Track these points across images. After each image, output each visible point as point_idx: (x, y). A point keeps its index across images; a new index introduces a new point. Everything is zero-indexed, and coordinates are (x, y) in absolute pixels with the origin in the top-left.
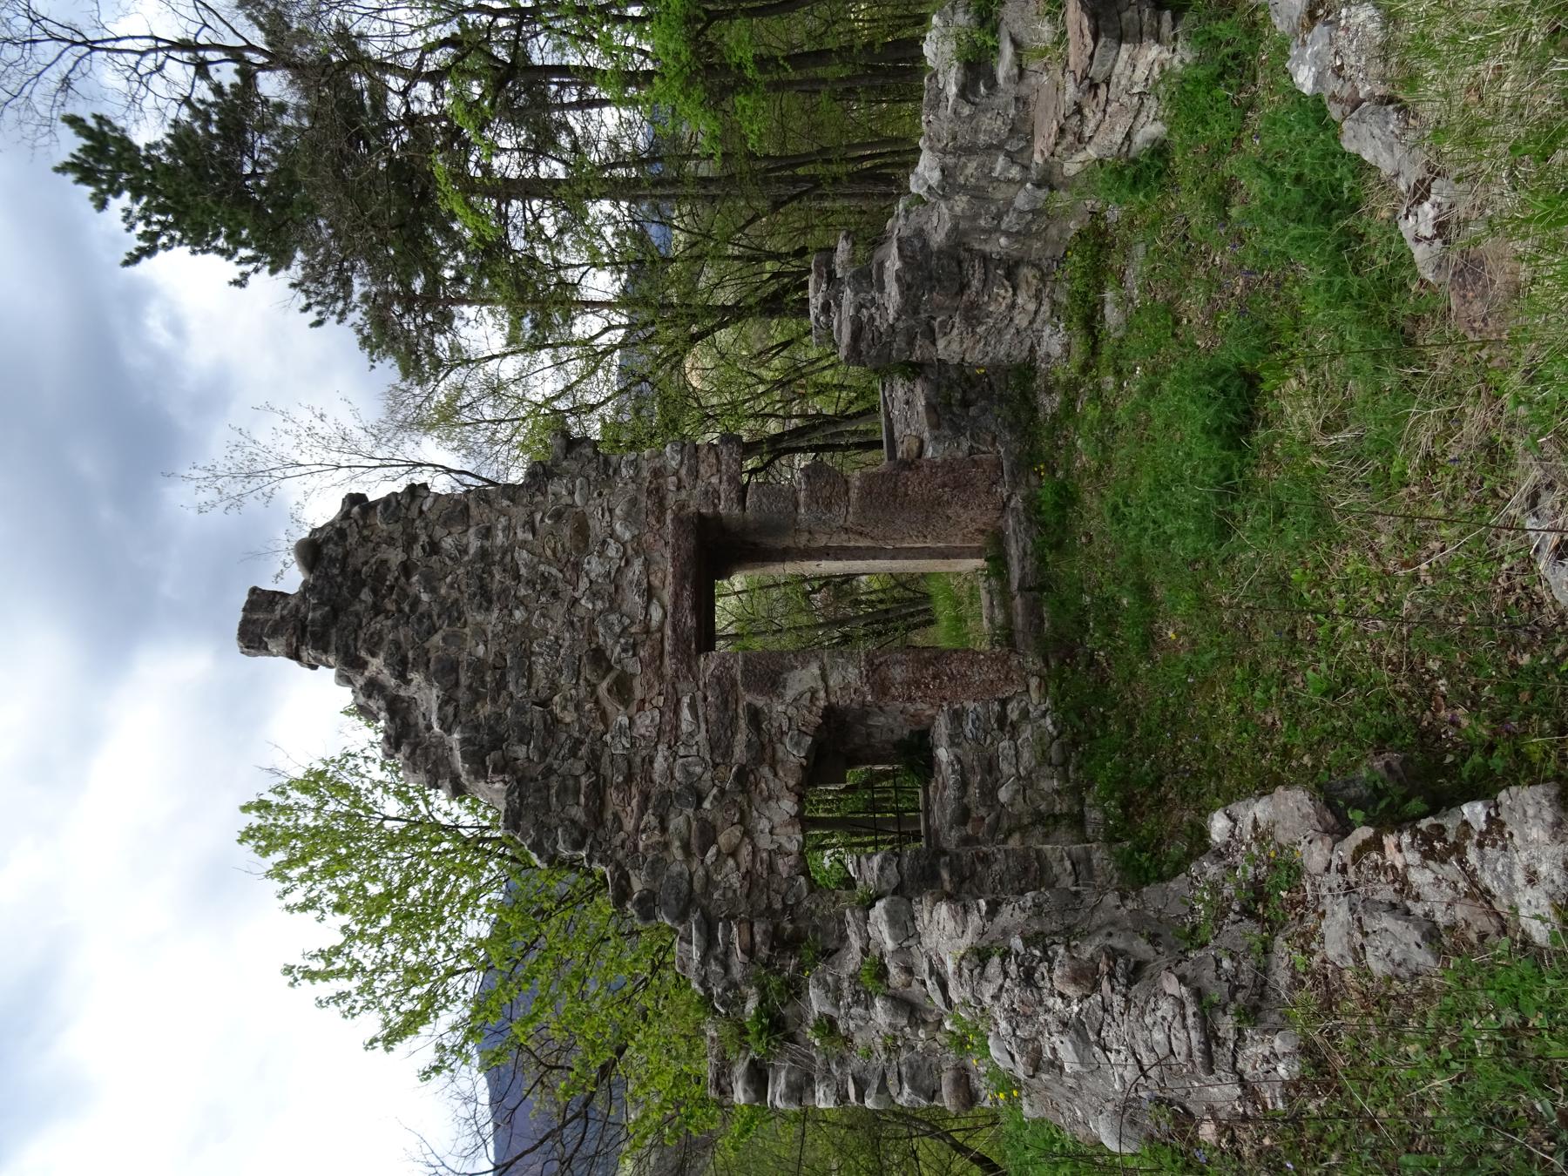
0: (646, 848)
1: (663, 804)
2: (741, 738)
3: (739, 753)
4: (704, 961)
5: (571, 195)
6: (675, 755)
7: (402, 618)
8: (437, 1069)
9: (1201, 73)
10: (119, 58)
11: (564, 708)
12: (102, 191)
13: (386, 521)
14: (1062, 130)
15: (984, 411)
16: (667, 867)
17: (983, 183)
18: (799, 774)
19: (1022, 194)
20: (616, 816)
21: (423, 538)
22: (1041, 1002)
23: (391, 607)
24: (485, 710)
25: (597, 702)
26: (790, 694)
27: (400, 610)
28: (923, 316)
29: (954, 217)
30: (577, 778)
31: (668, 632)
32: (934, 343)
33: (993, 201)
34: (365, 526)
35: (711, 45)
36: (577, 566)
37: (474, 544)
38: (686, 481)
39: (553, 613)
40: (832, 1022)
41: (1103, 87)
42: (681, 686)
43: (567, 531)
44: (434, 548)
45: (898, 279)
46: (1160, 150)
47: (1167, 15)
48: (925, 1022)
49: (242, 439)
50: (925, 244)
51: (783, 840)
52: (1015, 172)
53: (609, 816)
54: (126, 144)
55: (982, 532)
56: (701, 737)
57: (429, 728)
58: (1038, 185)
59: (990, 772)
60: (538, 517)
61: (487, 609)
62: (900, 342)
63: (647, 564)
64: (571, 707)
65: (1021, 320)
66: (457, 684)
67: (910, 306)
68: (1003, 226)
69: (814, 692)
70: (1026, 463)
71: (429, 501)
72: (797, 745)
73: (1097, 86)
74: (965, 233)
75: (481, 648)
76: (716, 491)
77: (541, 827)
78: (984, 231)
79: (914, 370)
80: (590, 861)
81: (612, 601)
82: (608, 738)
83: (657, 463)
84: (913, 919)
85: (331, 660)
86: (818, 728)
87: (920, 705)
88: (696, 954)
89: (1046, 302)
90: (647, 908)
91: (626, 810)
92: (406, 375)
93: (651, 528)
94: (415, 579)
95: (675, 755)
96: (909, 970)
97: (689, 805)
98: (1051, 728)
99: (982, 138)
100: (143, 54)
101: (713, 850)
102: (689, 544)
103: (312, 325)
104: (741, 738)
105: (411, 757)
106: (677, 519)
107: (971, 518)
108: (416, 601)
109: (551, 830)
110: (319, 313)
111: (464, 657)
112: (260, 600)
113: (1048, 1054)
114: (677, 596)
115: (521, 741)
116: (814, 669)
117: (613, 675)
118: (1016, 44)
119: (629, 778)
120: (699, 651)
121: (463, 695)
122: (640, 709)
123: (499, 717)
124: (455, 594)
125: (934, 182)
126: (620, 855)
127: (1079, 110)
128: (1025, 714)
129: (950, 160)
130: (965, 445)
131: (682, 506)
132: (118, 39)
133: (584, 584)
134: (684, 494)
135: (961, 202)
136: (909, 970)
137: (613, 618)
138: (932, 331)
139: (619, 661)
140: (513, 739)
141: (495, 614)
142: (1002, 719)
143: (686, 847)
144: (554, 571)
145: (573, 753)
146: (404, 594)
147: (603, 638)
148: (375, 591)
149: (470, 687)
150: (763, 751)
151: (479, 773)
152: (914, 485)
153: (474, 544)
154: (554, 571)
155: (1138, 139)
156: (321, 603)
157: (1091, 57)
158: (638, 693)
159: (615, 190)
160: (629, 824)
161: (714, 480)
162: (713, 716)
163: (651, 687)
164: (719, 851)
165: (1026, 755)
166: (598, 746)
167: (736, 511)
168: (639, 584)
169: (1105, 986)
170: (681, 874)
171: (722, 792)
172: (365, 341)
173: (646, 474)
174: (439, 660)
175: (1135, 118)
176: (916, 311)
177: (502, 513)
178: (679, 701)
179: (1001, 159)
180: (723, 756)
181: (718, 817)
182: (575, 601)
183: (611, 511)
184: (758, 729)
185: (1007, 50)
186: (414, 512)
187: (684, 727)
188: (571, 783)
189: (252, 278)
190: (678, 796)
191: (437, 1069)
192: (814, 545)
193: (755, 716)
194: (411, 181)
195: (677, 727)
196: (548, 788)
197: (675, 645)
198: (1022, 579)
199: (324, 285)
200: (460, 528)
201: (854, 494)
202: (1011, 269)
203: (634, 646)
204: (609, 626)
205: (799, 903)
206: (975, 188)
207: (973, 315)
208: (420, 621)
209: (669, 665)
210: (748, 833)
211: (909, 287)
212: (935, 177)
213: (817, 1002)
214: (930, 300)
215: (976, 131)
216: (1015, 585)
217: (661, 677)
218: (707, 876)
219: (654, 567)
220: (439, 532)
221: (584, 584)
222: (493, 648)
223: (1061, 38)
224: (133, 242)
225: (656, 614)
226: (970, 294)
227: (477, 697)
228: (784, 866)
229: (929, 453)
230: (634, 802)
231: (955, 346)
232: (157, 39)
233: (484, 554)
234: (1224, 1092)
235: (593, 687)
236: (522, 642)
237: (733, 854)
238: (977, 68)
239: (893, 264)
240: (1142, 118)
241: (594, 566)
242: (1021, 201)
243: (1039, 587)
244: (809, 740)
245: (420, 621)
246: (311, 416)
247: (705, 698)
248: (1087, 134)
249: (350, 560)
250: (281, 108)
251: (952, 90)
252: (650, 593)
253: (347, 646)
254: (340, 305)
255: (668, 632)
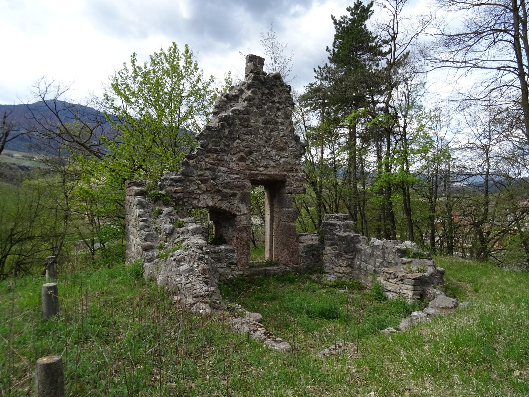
0: (201, 164)
1: (212, 169)
2: (229, 191)
3: (225, 191)
4: (171, 179)
5: (350, 146)
6: (224, 173)
7: (261, 100)
8: (107, 98)
9: (406, 305)
10: (392, 22)
11: (237, 143)
12: (352, 10)
13: (285, 97)
14: (390, 274)
15: (311, 260)
16: (196, 170)
17: (375, 256)
18: (219, 207)
19: (372, 266)
20: (209, 156)
21: (281, 107)
22: (195, 262)
23: (264, 98)
24: (237, 122)
25: (239, 152)
26: (240, 205)
27: (263, 100)
28: (338, 242)
29: (365, 250)
30: (219, 146)
31: (256, 172)
32: (330, 246)
33: (369, 259)
34: (284, 92)
35: (397, 189)
36: (273, 148)
37: (280, 120)
38: (294, 178)
39: (262, 141)
40: (161, 214)
41: (401, 282)
42: (242, 175)
43: (282, 145)
44: (279, 109)
45: (349, 235)
46: (386, 298)
47: (419, 297)
48: (167, 238)
49: (283, 47)
50: (357, 243)
51: (202, 202)
52: (378, 264)
53: (209, 154)
54: (367, 18)
55: (278, 260)
56: (229, 180)
57: (231, 106)
58: (374, 271)
59: (218, 260)
60: (286, 138)
61: (263, 123)
62: (330, 237)
63: (274, 167)
64: (238, 145)
65: (337, 269)
66: (244, 114)
67: (341, 239)
68: (362, 263)
69: (240, 211)
70: (297, 270)
71: (290, 109)
72: (227, 207)
73: (402, 281)
74: (360, 253)
75: (253, 121)
76: (291, 186)
77: (207, 136)
78: (361, 258)
79: (322, 241)
80: (197, 149)
81: (264, 157)
82: (229, 155)
83: (299, 170)
84: (197, 234)
85: (250, 81)
86: (231, 212)
87: (235, 241)
88: (173, 177)
89: (342, 275)
90: (186, 164)
91: (210, 159)
92: (301, 96)
93: (283, 168)
94: (271, 104)
95: (224, 173)
96: (182, 233)
97: (212, 176)
98: (229, 277)
99: (387, 255)
100: (393, 29)
101: (200, 183)
102: (279, 178)
103: (314, 69)
104: (229, 191)
105: (223, 101)
106: (285, 175)
107: (284, 257)
108: (265, 105)
109: (206, 139)
110: (318, 71)
111: (251, 117)
112: (261, 61)
113: (182, 264)
114: (265, 175)
115: (229, 131)
116: (246, 212)
117: (245, 156)
118: (411, 262)
119: (219, 160)
120: (251, 180)
121: (241, 116)
122: (237, 164)
123: (235, 125)
124: (267, 115)
125: (375, 244)
126: (199, 157)
127: (396, 277)
128: (233, 270)
129: (381, 247)
130: (302, 255)
131: (288, 177)
132: (397, 23)
133: (269, 150)
134: (291, 177)
135: (369, 251)
136: (182, 233)
137: (260, 157)
138: (334, 245)
139: (249, 159)
140: (231, 129)
141: (262, 126)
142: (232, 264)
143: (201, 175)
144: (272, 142)
145: (226, 145)
146: (267, 101)
147: (255, 154)
148: (268, 93)
149: (243, 118)
150: (225, 197)
151: (221, 120)
152: (293, 240)
153: (280, 120)
154: (272, 142)
155: (388, 293)
156: (265, 79)
157: (410, 279)
158: (240, 163)
159: (352, 159)
160: (207, 160)
161: (295, 186)
162: (235, 183)
163: (242, 167)
164: (200, 184)
165: (222, 270)
166: (227, 152)
167: (287, 191)
168: (269, 164)
169: (203, 276)
170: (194, 174)
171: (215, 186)
172: (312, 85)
173: (297, 167)
174: (250, 110)
175: (394, 292)
176: (339, 240)
177: (287, 128)
178: (238, 174)
179: (381, 260)
180: (224, 186)
181: (208, 184)
182: (265, 147)
183: (287, 157)
184: (231, 196)
185: (409, 260)
186: (288, 105)
187: (232, 176)
188: (218, 144)
189: (329, 53)
190: (215, 174)
191: (107, 98)
192: (274, 213)
193: (234, 195)
194: (360, 101)
195: (232, 174)
196: (217, 138)
197: (253, 174)
198: (268, 270)
199: (326, 73)
200: (283, 117)
201: (291, 224)
202: (351, 266)
203: (253, 163)
204: (258, 156)
205: (185, 206)
206: (373, 254)
207: (338, 256)
208: (260, 105)
209: (248, 172)
210: (204, 192)
211: (346, 238)
212: (376, 244)
213: (166, 210)
214: (343, 244)
215: (388, 253)
216: (267, 268)
217: (245, 170)
218: (193, 181)
219: (273, 168)
220: (283, 111)
221: (269, 150)
222: (253, 124)
223: (413, 272)
224: (338, 18)
225: (261, 169)
226: (344, 255)
227: (240, 120)
228: (195, 202)
229: (301, 245)
230: (212, 161)
231: (329, 252)
232: (397, 34)
233: (277, 123)
234: (190, 300)
235: (242, 151)
236: (254, 132)
237: (199, 188)
238: (404, 253)
239: (352, 234)
240: (393, 294)
241: (273, 152)
242: (370, 267)
243: (267, 275)
244: (228, 210)
245: (260, 105)
246: (290, 67)
247: (239, 182)
248: (389, 280)
249: (275, 87)
250: (378, 65)
251: (399, 247)
252: (266, 167)
253: (254, 85)
254: (320, 77)
255: (256, 172)
